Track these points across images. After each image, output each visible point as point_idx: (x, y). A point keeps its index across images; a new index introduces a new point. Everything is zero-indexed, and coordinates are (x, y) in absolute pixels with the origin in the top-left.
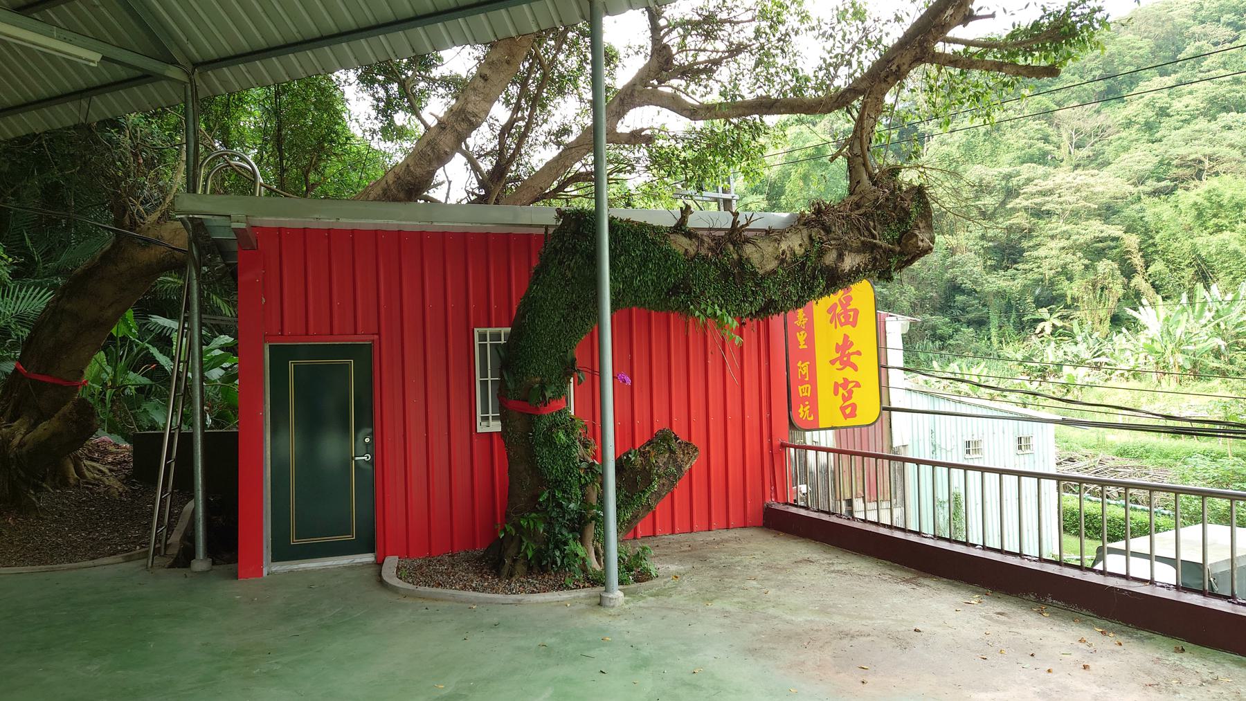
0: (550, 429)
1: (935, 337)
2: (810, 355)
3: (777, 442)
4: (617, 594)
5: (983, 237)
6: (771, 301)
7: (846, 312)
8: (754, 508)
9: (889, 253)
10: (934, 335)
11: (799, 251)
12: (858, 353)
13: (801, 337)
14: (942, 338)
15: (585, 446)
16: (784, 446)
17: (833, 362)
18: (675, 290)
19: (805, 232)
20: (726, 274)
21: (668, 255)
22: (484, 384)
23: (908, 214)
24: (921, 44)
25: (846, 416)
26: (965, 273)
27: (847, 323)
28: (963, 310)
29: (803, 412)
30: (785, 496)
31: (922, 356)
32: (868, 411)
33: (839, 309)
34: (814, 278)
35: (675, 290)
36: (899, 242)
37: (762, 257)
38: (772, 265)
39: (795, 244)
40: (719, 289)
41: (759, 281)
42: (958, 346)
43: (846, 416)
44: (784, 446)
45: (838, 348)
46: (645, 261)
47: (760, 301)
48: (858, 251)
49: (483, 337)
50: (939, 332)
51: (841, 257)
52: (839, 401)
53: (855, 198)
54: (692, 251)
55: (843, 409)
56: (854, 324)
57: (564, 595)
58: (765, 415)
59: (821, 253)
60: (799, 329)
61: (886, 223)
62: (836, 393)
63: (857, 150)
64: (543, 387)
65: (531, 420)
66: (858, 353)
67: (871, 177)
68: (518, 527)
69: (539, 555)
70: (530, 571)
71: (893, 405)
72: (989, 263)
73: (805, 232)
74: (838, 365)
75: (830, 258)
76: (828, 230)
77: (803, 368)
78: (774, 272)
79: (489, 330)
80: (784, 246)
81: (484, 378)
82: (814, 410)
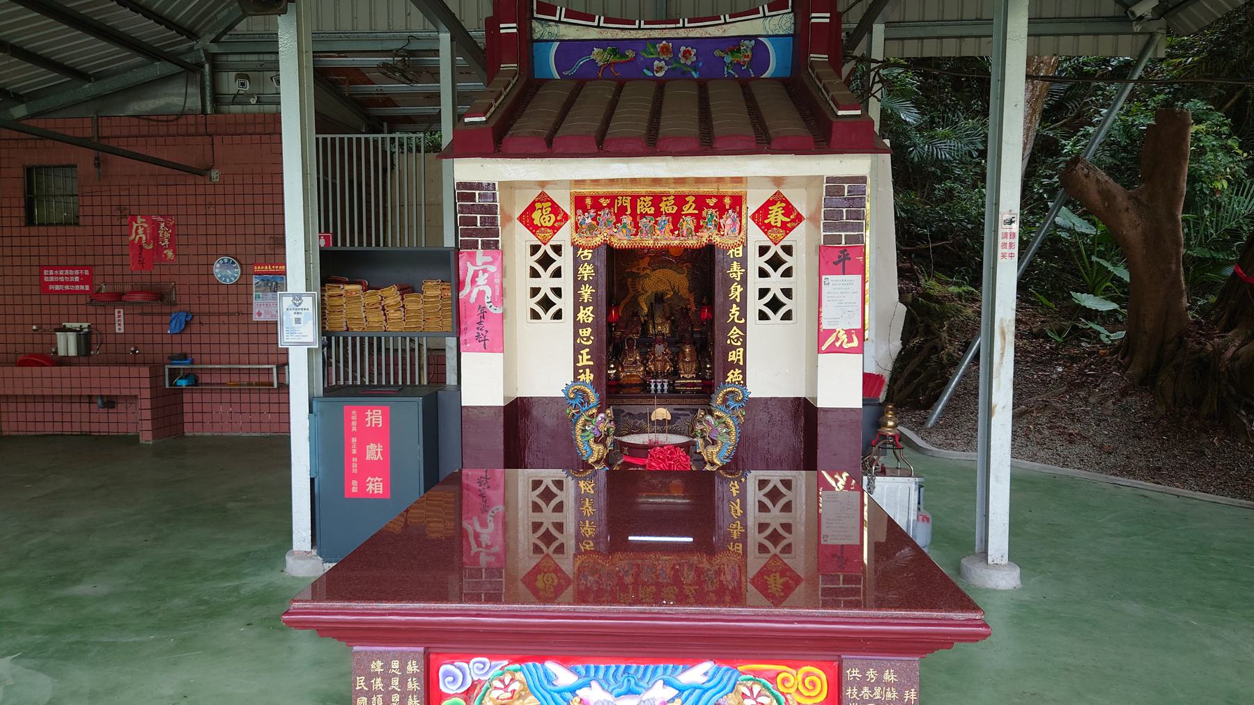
60: (863, 672)
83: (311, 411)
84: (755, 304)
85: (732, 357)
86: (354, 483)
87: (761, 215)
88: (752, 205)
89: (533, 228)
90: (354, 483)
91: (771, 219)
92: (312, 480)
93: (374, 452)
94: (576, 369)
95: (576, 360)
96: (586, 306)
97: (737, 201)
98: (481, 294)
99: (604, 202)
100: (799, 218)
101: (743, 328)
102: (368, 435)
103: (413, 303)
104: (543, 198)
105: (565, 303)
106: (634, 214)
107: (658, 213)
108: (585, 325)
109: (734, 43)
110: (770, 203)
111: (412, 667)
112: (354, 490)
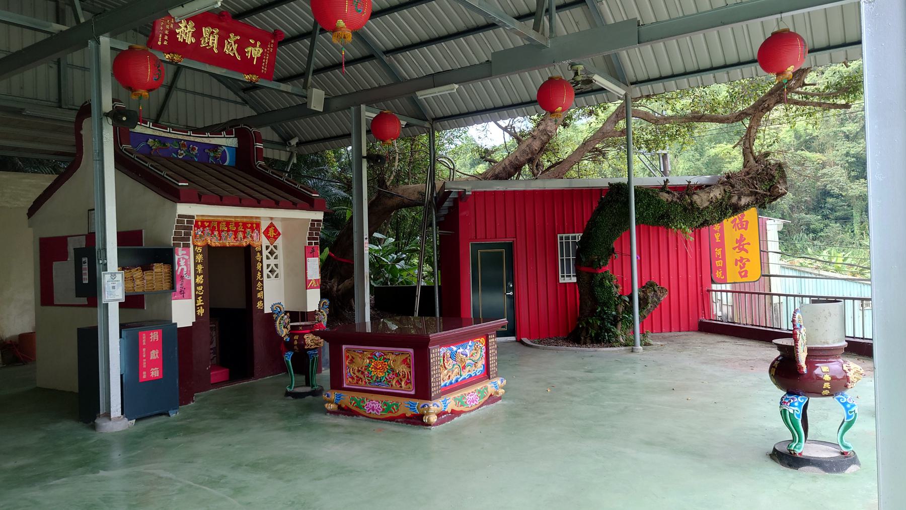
0: (602, 279)
1: (809, 230)
2: (722, 245)
3: (706, 289)
4: (639, 348)
5: (847, 154)
6: (706, 220)
7: (741, 223)
8: (694, 322)
9: (764, 196)
10: (808, 229)
11: (719, 197)
12: (748, 244)
13: (717, 236)
14: (814, 231)
15: (617, 287)
16: (709, 291)
17: (734, 249)
18: (662, 217)
19: (722, 188)
20: (685, 209)
21: (659, 202)
22: (562, 260)
23: (774, 177)
24: (779, 95)
25: (742, 277)
26: (833, 181)
27: (742, 228)
28: (832, 209)
29: (719, 274)
30: (709, 316)
31: (799, 246)
32: (754, 273)
33: (738, 221)
34: (727, 209)
35: (662, 217)
36: (769, 190)
37: (701, 200)
38: (706, 204)
39: (717, 193)
40: (674, 210)
41: (701, 212)
42: (828, 237)
43: (742, 277)
44: (709, 291)
45: (737, 241)
46: (649, 205)
47: (701, 220)
48: (748, 195)
49: (561, 238)
50: (812, 226)
51: (739, 198)
52: (738, 269)
53: (747, 170)
54: (670, 200)
55: (740, 273)
56: (746, 229)
57: (612, 349)
58: (699, 275)
59: (730, 198)
60: (716, 232)
61: (762, 181)
62: (736, 264)
63: (747, 145)
64: (599, 261)
65: (592, 276)
66: (748, 244)
67: (755, 158)
68: (588, 323)
69: (597, 335)
70: (592, 342)
71: (771, 273)
72: (853, 174)
73: (722, 188)
74: (737, 250)
75: (734, 200)
76: (733, 186)
77: (718, 252)
78: (708, 207)
79: (564, 235)
80: (712, 195)
81: (566, 258)
82: (724, 273)
83: (121, 337)
84: (266, 271)
85: (259, 295)
86: (144, 373)
87: (266, 232)
88: (263, 228)
89: (268, 238)
90: (144, 373)
91: (270, 234)
92: (122, 376)
93: (154, 354)
94: (196, 307)
95: (196, 303)
96: (200, 275)
97: (258, 226)
98: (182, 269)
99: (207, 224)
100: (279, 234)
101: (262, 282)
102: (151, 346)
103: (148, 276)
104: (271, 225)
105: (281, 271)
106: (218, 230)
107: (228, 231)
108: (200, 285)
109: (216, 147)
110: (269, 227)
111: (443, 350)
112: (144, 377)
